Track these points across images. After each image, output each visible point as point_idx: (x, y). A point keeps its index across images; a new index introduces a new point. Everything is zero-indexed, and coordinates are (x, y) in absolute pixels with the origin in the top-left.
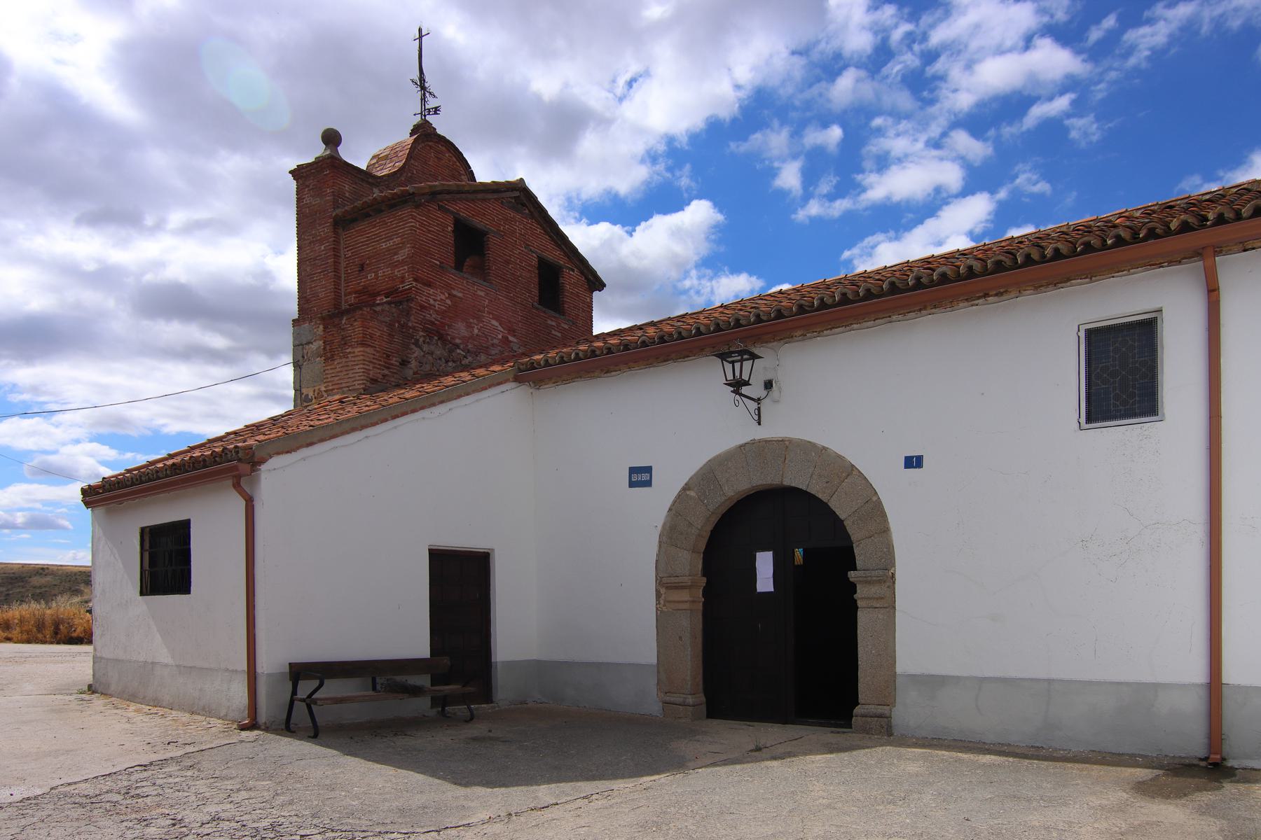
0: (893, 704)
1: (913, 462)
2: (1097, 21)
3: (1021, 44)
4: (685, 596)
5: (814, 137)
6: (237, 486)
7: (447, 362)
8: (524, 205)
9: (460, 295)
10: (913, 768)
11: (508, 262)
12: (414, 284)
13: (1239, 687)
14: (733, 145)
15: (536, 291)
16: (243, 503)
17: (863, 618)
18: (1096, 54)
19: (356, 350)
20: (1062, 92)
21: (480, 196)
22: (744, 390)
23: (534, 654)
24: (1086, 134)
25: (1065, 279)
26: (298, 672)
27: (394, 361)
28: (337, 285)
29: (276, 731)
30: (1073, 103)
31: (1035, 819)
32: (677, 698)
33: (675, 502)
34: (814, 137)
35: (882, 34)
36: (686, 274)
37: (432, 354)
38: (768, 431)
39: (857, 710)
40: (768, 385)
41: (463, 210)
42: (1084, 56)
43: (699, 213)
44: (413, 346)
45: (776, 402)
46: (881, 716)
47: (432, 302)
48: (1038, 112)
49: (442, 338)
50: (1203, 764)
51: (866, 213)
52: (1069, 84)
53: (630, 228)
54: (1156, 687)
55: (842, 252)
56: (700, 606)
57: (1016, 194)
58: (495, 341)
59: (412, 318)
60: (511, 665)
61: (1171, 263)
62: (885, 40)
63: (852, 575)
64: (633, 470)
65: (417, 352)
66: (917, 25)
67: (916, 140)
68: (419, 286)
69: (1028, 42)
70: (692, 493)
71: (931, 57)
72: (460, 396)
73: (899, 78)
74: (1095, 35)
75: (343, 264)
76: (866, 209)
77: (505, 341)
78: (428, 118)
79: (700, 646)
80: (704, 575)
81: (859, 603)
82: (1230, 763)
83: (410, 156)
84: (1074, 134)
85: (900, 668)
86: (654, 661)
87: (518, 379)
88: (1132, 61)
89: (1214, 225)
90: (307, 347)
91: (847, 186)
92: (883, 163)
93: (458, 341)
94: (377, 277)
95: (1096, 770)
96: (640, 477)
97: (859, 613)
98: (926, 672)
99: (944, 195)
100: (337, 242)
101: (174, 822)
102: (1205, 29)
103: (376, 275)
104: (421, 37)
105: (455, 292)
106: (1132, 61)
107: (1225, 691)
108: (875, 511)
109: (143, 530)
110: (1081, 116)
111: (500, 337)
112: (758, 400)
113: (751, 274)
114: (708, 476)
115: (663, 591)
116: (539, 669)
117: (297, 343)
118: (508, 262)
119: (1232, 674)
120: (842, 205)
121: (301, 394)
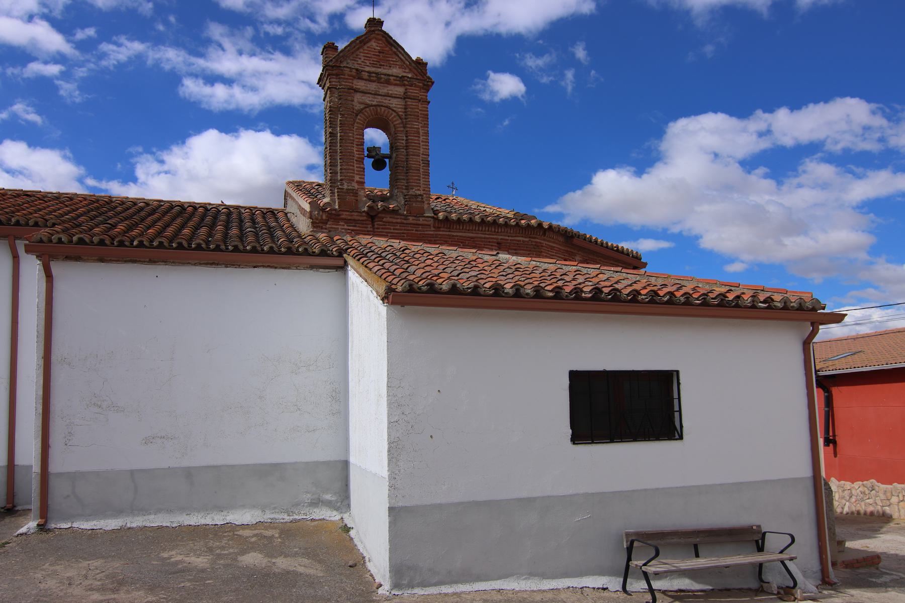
2: (83, 27)
13: (23, 466)
18: (84, 46)
30: (62, 73)
48: (35, 68)
50: (2, 510)
52: (58, 58)
57: (15, 116)
69: (30, 18)
82: (19, 508)
88: (104, 63)
89: (14, 225)
101: (407, 175)
106: (104, 63)
107: (16, 469)
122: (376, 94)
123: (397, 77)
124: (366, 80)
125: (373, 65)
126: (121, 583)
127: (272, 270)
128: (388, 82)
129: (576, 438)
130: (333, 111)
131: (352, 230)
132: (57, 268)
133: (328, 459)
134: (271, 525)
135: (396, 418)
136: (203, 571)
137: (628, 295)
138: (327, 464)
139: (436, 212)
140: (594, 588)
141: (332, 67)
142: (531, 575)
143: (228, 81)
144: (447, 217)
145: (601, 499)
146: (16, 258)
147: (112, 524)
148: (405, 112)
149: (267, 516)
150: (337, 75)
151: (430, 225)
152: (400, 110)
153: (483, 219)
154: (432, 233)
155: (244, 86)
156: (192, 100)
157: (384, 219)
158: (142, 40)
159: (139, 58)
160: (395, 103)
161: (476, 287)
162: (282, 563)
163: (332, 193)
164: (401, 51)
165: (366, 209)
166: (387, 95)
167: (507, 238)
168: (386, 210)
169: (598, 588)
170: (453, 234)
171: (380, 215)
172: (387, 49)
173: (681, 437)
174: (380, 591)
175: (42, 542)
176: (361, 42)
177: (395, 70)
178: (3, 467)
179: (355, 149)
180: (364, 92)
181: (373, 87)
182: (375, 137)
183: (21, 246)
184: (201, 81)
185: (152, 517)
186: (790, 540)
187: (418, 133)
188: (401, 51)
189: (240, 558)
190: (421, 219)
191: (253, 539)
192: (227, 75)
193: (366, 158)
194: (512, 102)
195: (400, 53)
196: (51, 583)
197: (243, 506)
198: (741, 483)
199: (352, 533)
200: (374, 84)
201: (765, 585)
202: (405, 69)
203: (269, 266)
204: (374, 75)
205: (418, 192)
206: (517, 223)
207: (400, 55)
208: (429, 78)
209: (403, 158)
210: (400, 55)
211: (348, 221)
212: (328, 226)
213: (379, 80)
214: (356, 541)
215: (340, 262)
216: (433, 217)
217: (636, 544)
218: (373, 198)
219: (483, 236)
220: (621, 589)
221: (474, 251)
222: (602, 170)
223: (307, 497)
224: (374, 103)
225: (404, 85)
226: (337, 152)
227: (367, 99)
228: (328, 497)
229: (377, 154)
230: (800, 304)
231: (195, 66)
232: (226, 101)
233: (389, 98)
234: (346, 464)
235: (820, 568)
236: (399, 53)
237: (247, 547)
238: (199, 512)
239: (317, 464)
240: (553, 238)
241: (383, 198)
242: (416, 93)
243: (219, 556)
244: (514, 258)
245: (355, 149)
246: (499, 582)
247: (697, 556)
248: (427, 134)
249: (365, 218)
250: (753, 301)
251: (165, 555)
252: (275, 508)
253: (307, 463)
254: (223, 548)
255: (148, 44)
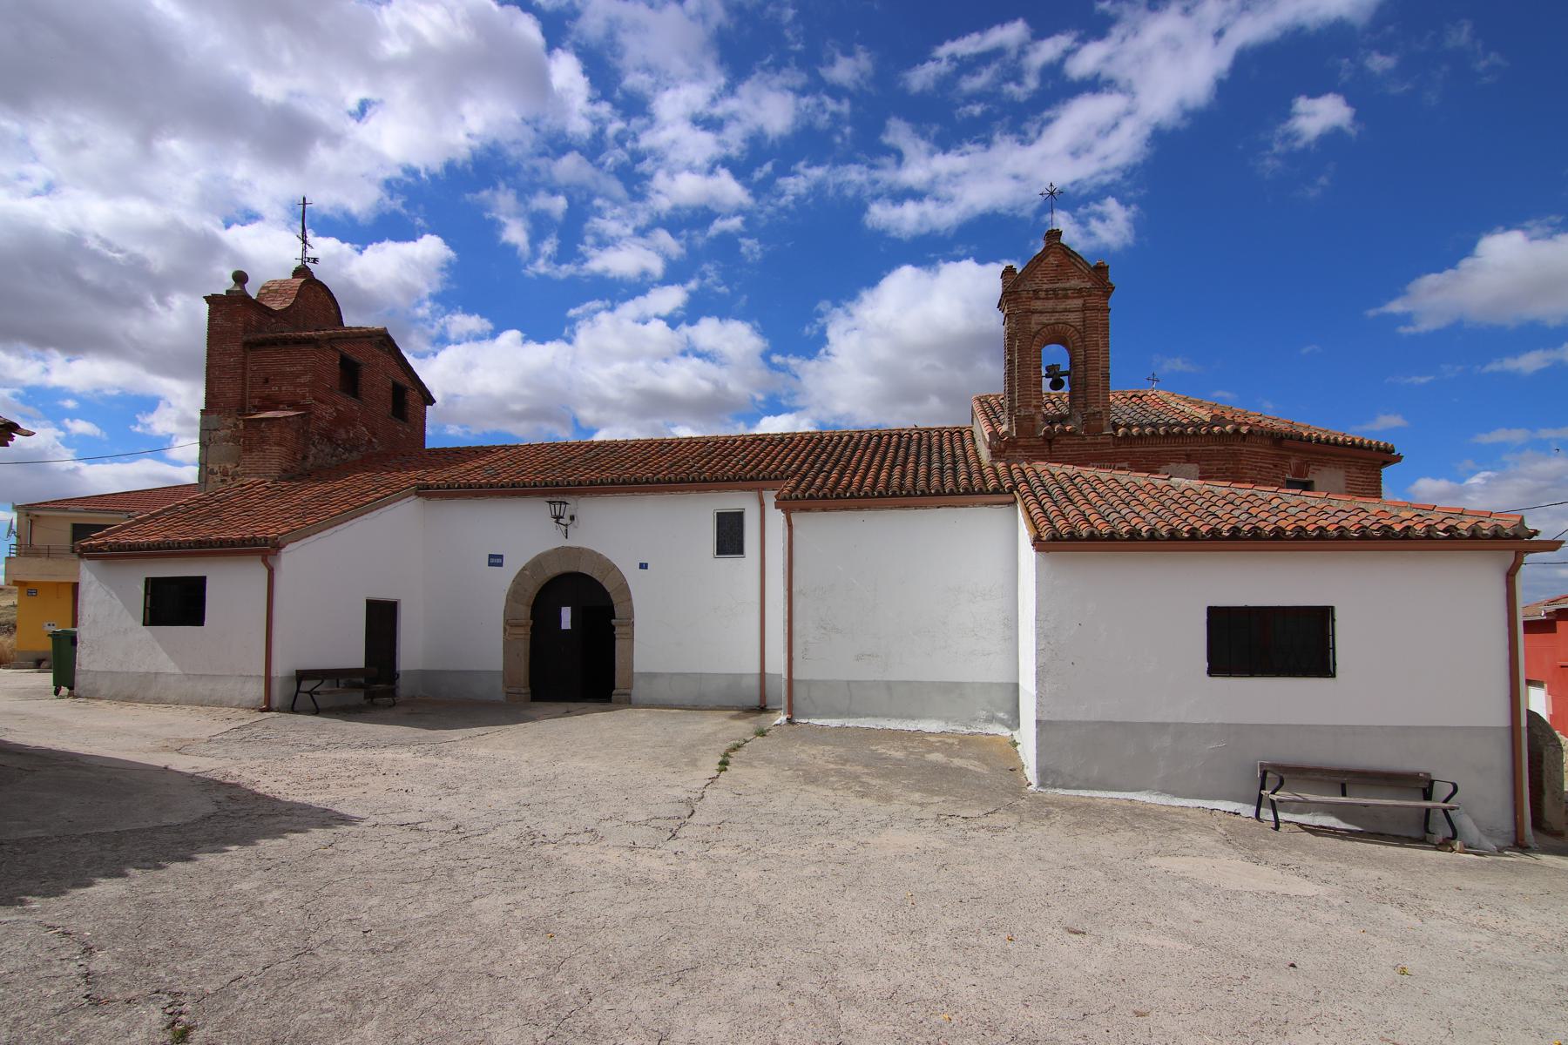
0: (631, 688)
1: (643, 566)
2: (761, 165)
3: (707, 166)
4: (521, 631)
5: (542, 202)
6: (265, 561)
7: (332, 456)
8: (385, 345)
9: (342, 409)
10: (643, 715)
11: (373, 385)
12: (313, 401)
14: (468, 197)
15: (390, 406)
16: (267, 571)
17: (618, 644)
18: (759, 190)
19: (274, 448)
20: (736, 215)
21: (358, 340)
22: (561, 521)
23: (420, 666)
24: (752, 252)
25: (707, 490)
26: (302, 676)
27: (299, 456)
28: (244, 389)
29: (288, 712)
31: (690, 727)
32: (515, 690)
33: (516, 577)
34: (542, 202)
35: (599, 124)
36: (420, 304)
37: (322, 451)
38: (573, 542)
39: (614, 692)
40: (572, 518)
41: (346, 349)
42: (750, 191)
43: (430, 248)
44: (311, 446)
45: (576, 527)
46: (625, 694)
47: (324, 414)
48: (719, 226)
49: (330, 439)
51: (587, 280)
53: (359, 247)
54: (741, 675)
55: (568, 310)
56: (529, 637)
58: (363, 442)
59: (311, 426)
60: (408, 672)
61: (748, 490)
62: (602, 131)
63: (613, 621)
64: (491, 556)
65: (313, 450)
66: (628, 124)
67: (626, 225)
68: (317, 403)
70: (527, 573)
71: (638, 157)
72: (386, 505)
73: (612, 169)
74: (758, 175)
75: (249, 375)
76: (587, 277)
77: (370, 441)
78: (307, 264)
79: (528, 661)
80: (531, 618)
81: (617, 636)
82: (767, 708)
83: (298, 295)
84: (743, 250)
85: (635, 670)
86: (502, 669)
87: (418, 494)
88: (783, 202)
90: (214, 432)
91: (569, 251)
92: (603, 243)
93: (340, 442)
94: (280, 390)
95: (717, 713)
96: (496, 560)
97: (617, 641)
98: (648, 671)
99: (650, 279)
100: (245, 358)
102: (831, 192)
103: (280, 388)
104: (304, 204)
105: (339, 407)
106: (783, 202)
108: (624, 589)
109: (147, 579)
110: (750, 238)
111: (366, 439)
112: (566, 525)
113: (482, 316)
114: (537, 563)
115: (508, 627)
116: (424, 675)
117: (205, 428)
118: (373, 385)
119: (768, 670)
120: (567, 270)
121: (207, 468)
122: (1054, 311)
123: (1075, 290)
124: (1043, 299)
125: (1051, 281)
126: (846, 761)
127: (953, 509)
128: (1066, 297)
129: (1214, 670)
130: (1011, 337)
131: (1030, 456)
132: (795, 517)
133: (1000, 681)
134: (953, 734)
135: (1043, 647)
136: (900, 760)
137: (1270, 532)
138: (1000, 685)
139: (1115, 427)
140: (1225, 811)
141: (1010, 293)
142: (1163, 791)
143: (914, 194)
144: (1127, 434)
145: (1235, 731)
146: (762, 505)
147: (835, 723)
148: (1084, 325)
149: (950, 728)
150: (1015, 299)
151: (1109, 443)
152: (1078, 324)
153: (1167, 431)
154: (1111, 451)
155: (937, 199)
156: (881, 229)
157: (1062, 442)
158: (818, 162)
159: (818, 189)
160: (1074, 318)
161: (1112, 533)
162: (957, 762)
163: (1011, 421)
164: (1080, 260)
165: (1042, 434)
166: (1066, 310)
167: (1198, 448)
168: (1063, 433)
169: (1230, 812)
170: (1136, 450)
171: (1057, 438)
172: (1065, 261)
173: (1334, 676)
174: (1029, 788)
175: (791, 731)
176: (1038, 260)
177: (1073, 282)
178: (755, 674)
179: (1032, 373)
180: (1041, 312)
181: (1050, 304)
182: (1054, 355)
183: (770, 498)
184: (889, 203)
185: (863, 720)
186: (1451, 789)
187: (1097, 345)
188: (1080, 260)
189: (926, 756)
190: (1099, 437)
191: (937, 744)
192: (917, 187)
193: (1044, 378)
194: (1332, 139)
195: (1079, 262)
196: (803, 756)
197: (931, 717)
198: (1409, 727)
199: (1019, 748)
200: (1052, 301)
201: (1428, 835)
202: (1084, 278)
203: (950, 506)
204: (1051, 292)
205: (1097, 409)
206: (1208, 432)
207: (1079, 265)
208: (1110, 284)
209: (1081, 374)
210: (1079, 265)
211: (1025, 448)
212: (1006, 454)
213: (1056, 297)
214: (1020, 754)
215: (1010, 498)
216: (1111, 434)
217: (1269, 775)
218: (1051, 421)
219: (1169, 449)
220: (1254, 816)
221: (1146, 475)
222: (1501, 228)
223: (983, 714)
224: (1052, 321)
225: (1083, 296)
226: (1014, 379)
227: (1044, 319)
228: (1001, 715)
229: (1055, 373)
230: (1496, 531)
231: (880, 184)
232: (920, 224)
233: (1066, 314)
234: (1017, 685)
235: (1514, 829)
236: (1076, 263)
237: (932, 748)
238: (896, 718)
239: (991, 684)
240: (1256, 443)
241: (1062, 419)
242: (1096, 303)
243: (912, 753)
244: (1187, 482)
245: (1032, 373)
246: (1131, 793)
247: (1344, 794)
248: (1107, 345)
249: (1042, 443)
250: (1428, 531)
251: (873, 748)
252: (956, 721)
253: (983, 683)
254: (914, 748)
255: (827, 167)
